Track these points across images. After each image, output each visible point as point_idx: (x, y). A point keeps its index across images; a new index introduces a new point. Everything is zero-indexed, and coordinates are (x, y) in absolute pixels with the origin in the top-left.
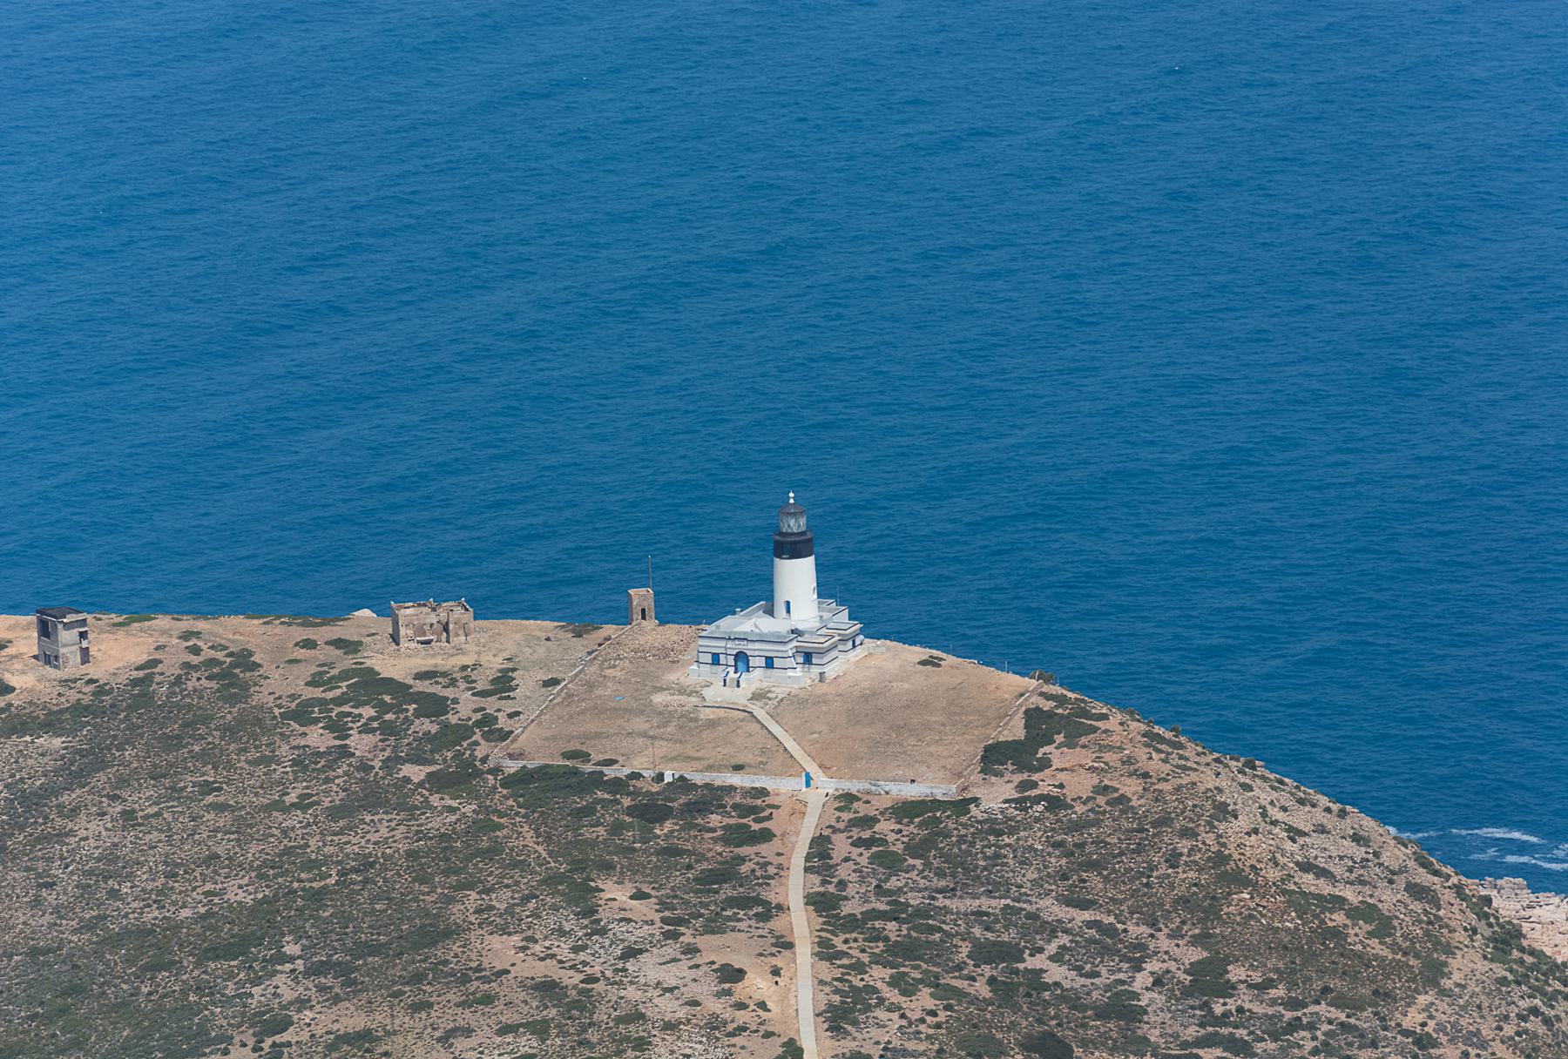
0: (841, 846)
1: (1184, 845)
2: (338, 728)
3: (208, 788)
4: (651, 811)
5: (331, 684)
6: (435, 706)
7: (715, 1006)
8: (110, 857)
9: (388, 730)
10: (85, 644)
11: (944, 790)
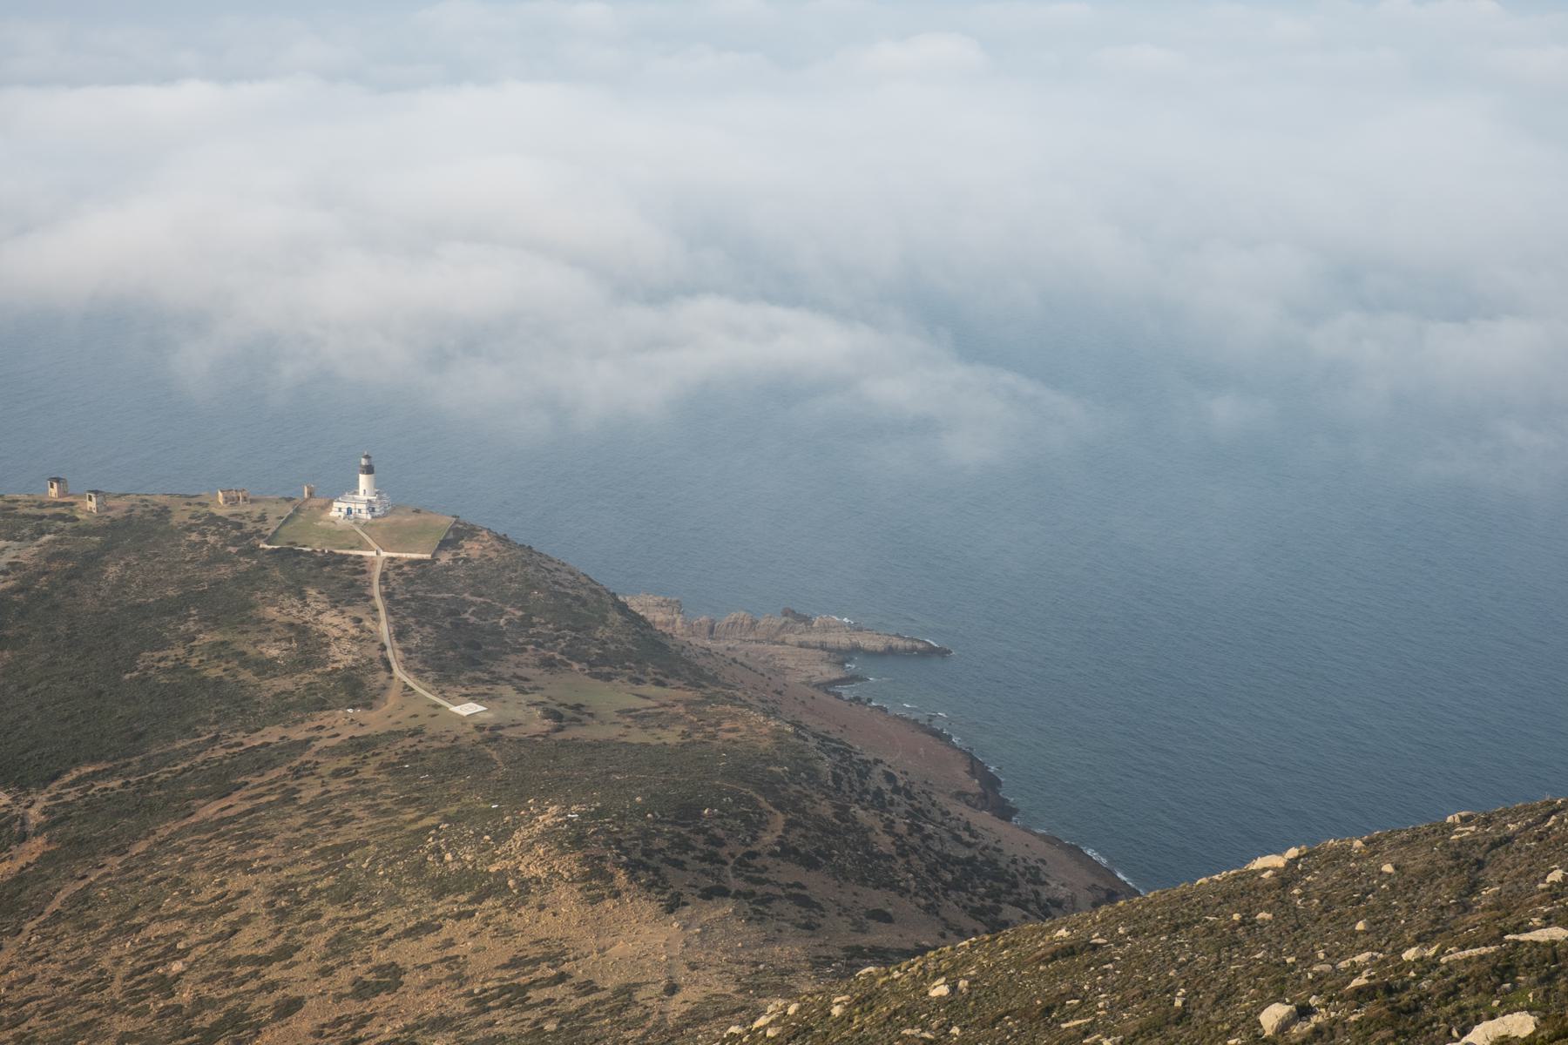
0: (391, 575)
1: (513, 575)
2: (203, 534)
3: (156, 555)
4: (323, 563)
5: (199, 518)
6: (239, 526)
7: (354, 632)
8: (121, 579)
9: (221, 534)
10: (1380, 993)
11: (427, 556)
